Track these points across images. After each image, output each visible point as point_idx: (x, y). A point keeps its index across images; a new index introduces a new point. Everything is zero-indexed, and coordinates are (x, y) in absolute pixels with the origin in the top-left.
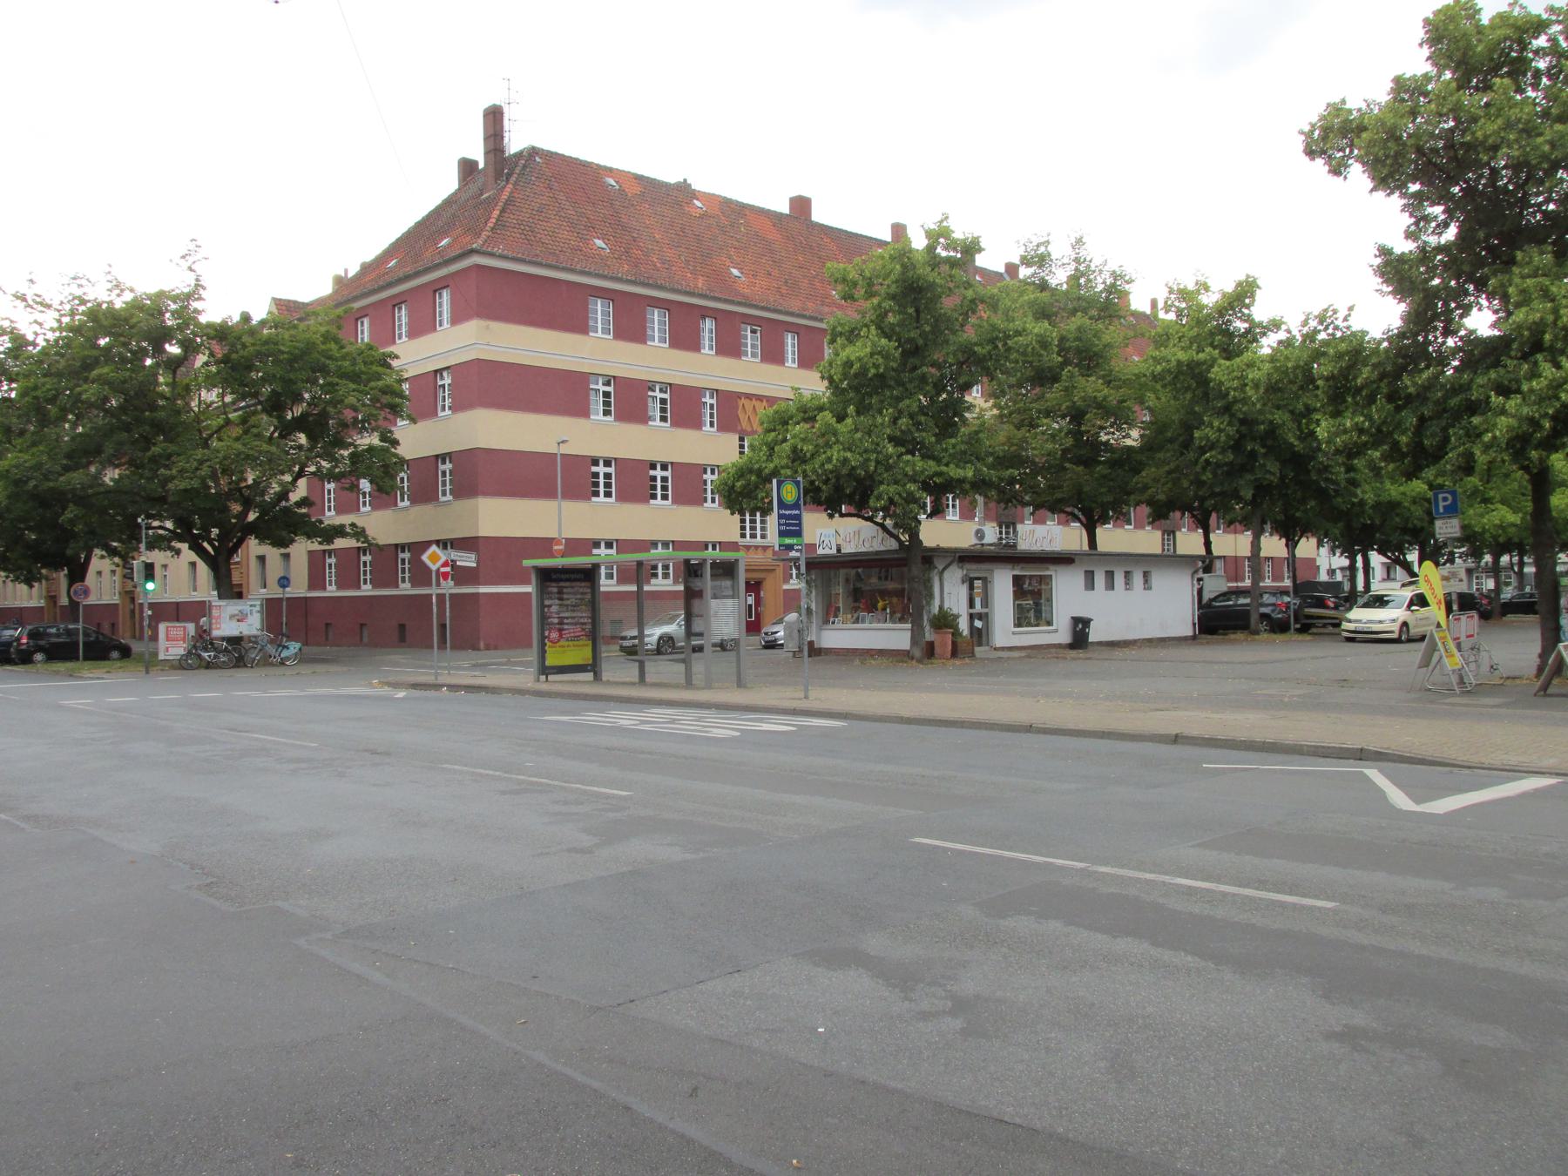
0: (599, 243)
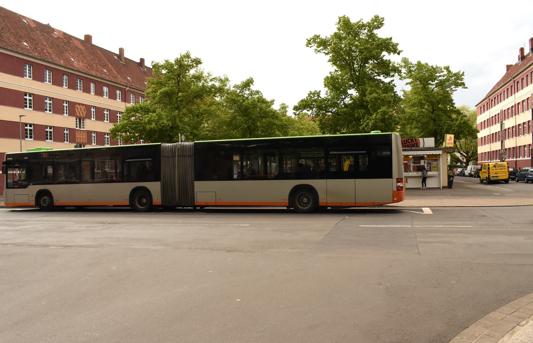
0: (25, 44)
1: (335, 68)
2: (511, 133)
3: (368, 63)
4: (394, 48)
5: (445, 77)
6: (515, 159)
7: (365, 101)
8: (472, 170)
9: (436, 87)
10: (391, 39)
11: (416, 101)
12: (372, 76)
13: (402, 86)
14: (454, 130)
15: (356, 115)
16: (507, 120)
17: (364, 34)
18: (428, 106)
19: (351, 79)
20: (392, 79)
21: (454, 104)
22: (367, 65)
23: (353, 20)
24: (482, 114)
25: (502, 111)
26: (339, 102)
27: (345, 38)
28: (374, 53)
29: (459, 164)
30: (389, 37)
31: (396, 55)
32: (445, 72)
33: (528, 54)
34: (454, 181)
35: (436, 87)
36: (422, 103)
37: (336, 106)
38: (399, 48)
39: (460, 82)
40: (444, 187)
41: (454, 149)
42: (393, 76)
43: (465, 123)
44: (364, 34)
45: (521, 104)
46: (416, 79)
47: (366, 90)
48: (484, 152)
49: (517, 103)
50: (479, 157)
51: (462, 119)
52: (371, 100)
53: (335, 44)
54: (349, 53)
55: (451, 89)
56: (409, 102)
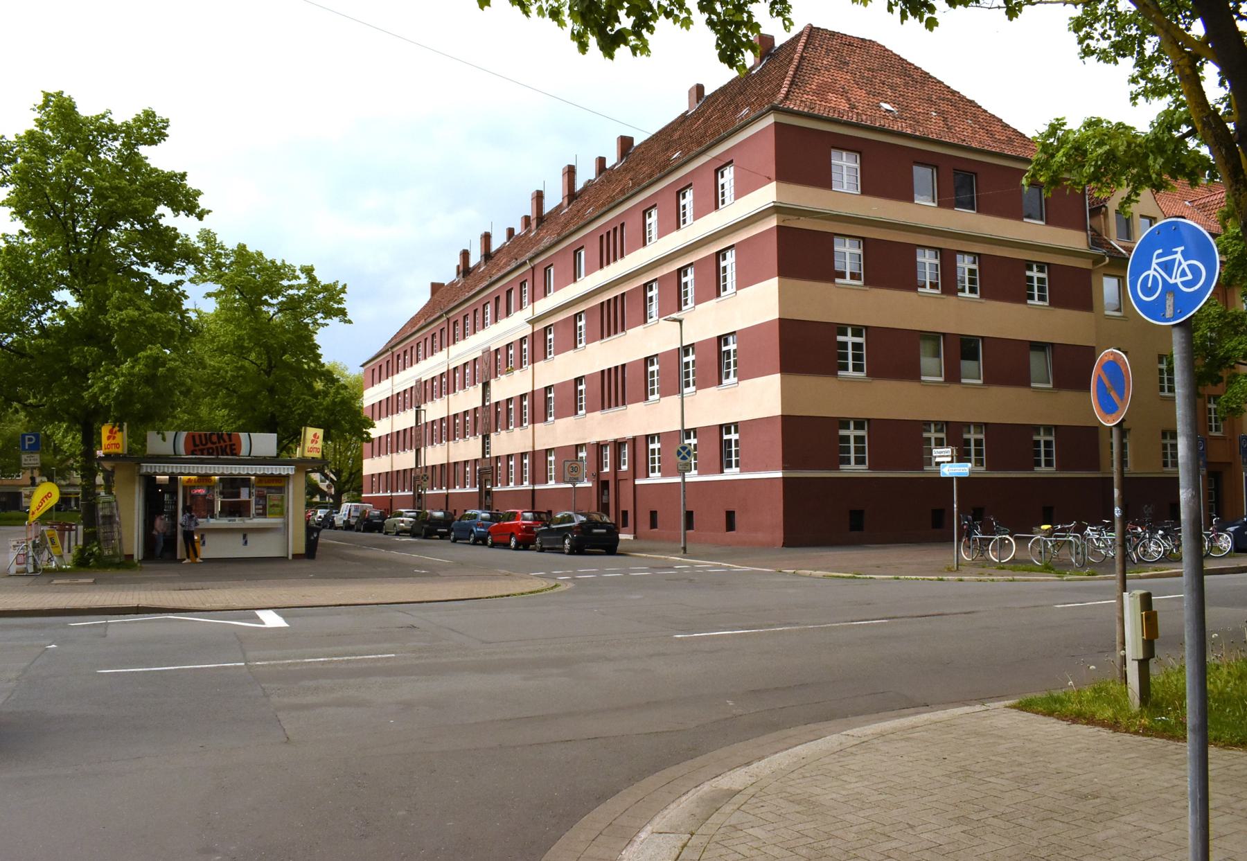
1: (20, 225)
2: (460, 428)
3: (115, 226)
4: (188, 201)
5: (303, 291)
6: (444, 491)
7: (102, 326)
8: (352, 514)
9: (280, 311)
10: (183, 176)
11: (229, 339)
12: (127, 263)
13: (201, 299)
14: (319, 417)
15: (75, 360)
16: (429, 404)
17: (110, 151)
18: (259, 354)
19: (66, 260)
20: (179, 277)
21: (320, 356)
22: (113, 231)
23: (86, 109)
24: (376, 386)
25: (419, 381)
26: (25, 319)
27: (56, 151)
28: (137, 203)
29: (317, 499)
30: (179, 170)
31: (193, 218)
32: (304, 280)
33: (478, 266)
34: (321, 541)
35: (280, 311)
36: (242, 347)
37: (17, 331)
38: (202, 202)
39: (336, 306)
40: (296, 556)
41: (319, 465)
42: (181, 271)
43: (344, 402)
44: (110, 151)
45: (461, 370)
46: (231, 286)
47: (108, 297)
48: (376, 472)
49: (451, 367)
50: (366, 485)
51: (337, 393)
52: (119, 325)
53: (26, 160)
54: (67, 191)
55: (315, 322)
56: (212, 341)
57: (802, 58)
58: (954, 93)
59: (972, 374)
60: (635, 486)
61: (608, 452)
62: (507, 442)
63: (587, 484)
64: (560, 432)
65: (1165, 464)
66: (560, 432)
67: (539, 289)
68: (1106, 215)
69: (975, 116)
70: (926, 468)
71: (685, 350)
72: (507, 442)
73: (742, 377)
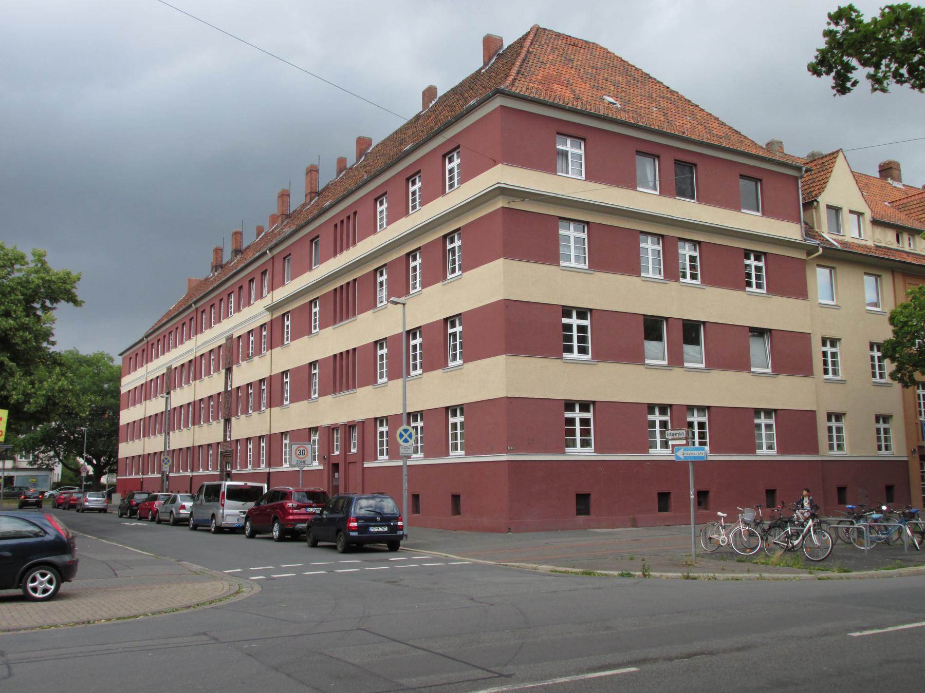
57: (528, 51)
58: (673, 92)
59: (694, 355)
60: (364, 469)
61: (338, 436)
62: (245, 426)
63: (316, 465)
64: (293, 416)
65: (880, 448)
66: (293, 416)
67: (277, 279)
68: (817, 208)
69: (693, 113)
70: (758, 452)
71: (412, 333)
72: (245, 426)
73: (467, 359)
